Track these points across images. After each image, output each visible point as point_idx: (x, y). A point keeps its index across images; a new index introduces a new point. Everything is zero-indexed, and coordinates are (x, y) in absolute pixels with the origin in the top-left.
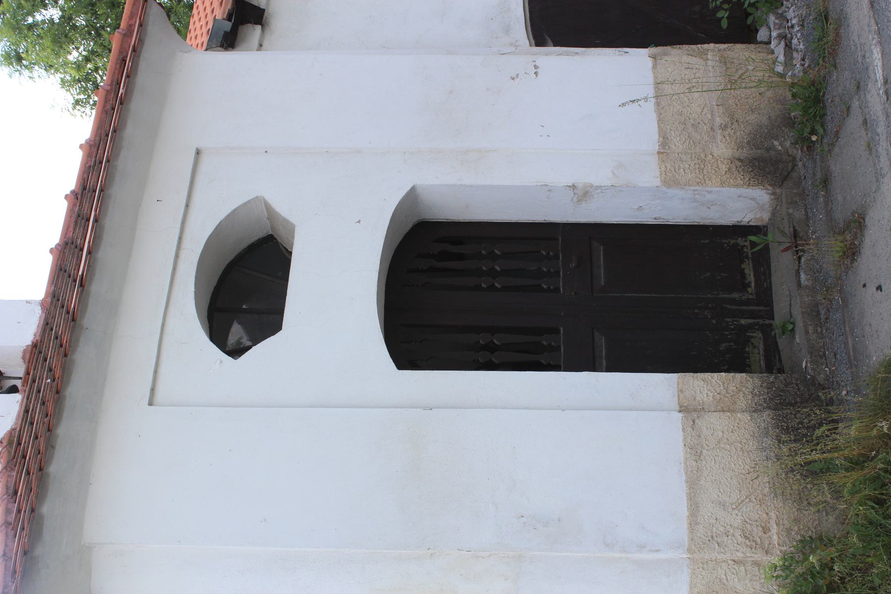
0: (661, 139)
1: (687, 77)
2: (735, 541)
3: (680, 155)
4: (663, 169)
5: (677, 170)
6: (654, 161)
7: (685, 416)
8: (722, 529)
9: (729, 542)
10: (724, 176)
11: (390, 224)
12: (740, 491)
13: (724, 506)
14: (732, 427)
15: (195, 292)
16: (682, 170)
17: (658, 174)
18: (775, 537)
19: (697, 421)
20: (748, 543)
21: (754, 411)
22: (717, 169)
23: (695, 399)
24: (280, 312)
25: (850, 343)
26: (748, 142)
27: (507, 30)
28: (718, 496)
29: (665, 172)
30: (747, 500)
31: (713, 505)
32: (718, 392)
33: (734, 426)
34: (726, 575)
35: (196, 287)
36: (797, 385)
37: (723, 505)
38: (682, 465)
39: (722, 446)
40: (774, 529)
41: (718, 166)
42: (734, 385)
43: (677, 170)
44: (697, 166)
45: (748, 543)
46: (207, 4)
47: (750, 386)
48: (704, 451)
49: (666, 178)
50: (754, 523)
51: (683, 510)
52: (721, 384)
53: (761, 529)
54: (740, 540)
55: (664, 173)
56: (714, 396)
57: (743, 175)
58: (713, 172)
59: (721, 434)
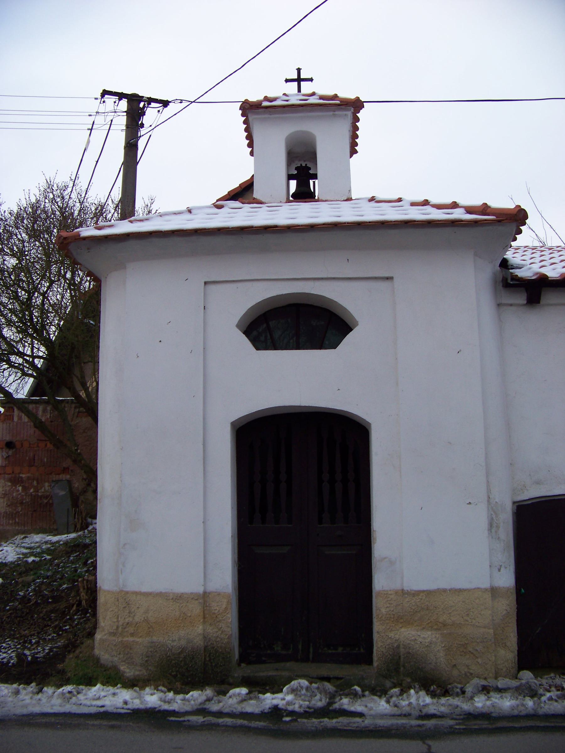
0: (413, 592)
1: (471, 613)
2: (126, 617)
3: (401, 605)
4: (390, 592)
5: (389, 602)
6: (397, 586)
7: (200, 595)
8: (133, 610)
9: (126, 614)
10: (384, 634)
11: (338, 410)
12: (155, 623)
13: (146, 613)
14: (194, 622)
15: (283, 295)
16: (388, 605)
17: (384, 589)
18: (127, 639)
19: (197, 602)
20: (125, 624)
21: (204, 637)
22: (390, 630)
23: (213, 602)
24: (275, 346)
25: (334, 720)
26: (409, 653)
27: (538, 483)
28: (152, 610)
29: (387, 594)
30: (149, 626)
31: (147, 606)
32: (218, 616)
33: (194, 623)
34: (112, 611)
35: (285, 294)
36: (224, 665)
37: (147, 612)
38: (171, 591)
39: (182, 615)
40: (131, 639)
41: (393, 631)
42: (223, 626)
43: (389, 602)
44: (392, 616)
45: (125, 624)
46: (562, 258)
47: (222, 636)
48: (178, 604)
49: (382, 594)
50: (136, 628)
51: (144, 589)
52: (224, 618)
53: (132, 632)
54: (127, 620)
55: (386, 593)
56: (215, 613)
57: (385, 647)
58: (388, 627)
59: (189, 615)
